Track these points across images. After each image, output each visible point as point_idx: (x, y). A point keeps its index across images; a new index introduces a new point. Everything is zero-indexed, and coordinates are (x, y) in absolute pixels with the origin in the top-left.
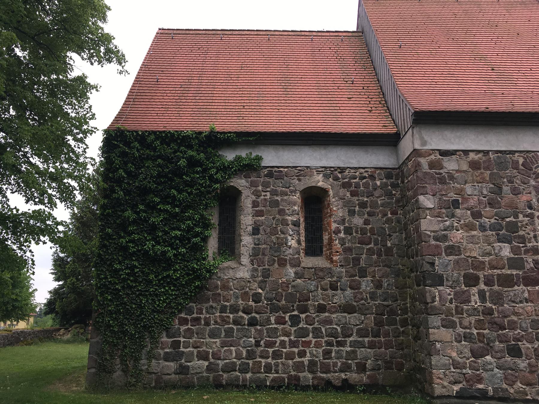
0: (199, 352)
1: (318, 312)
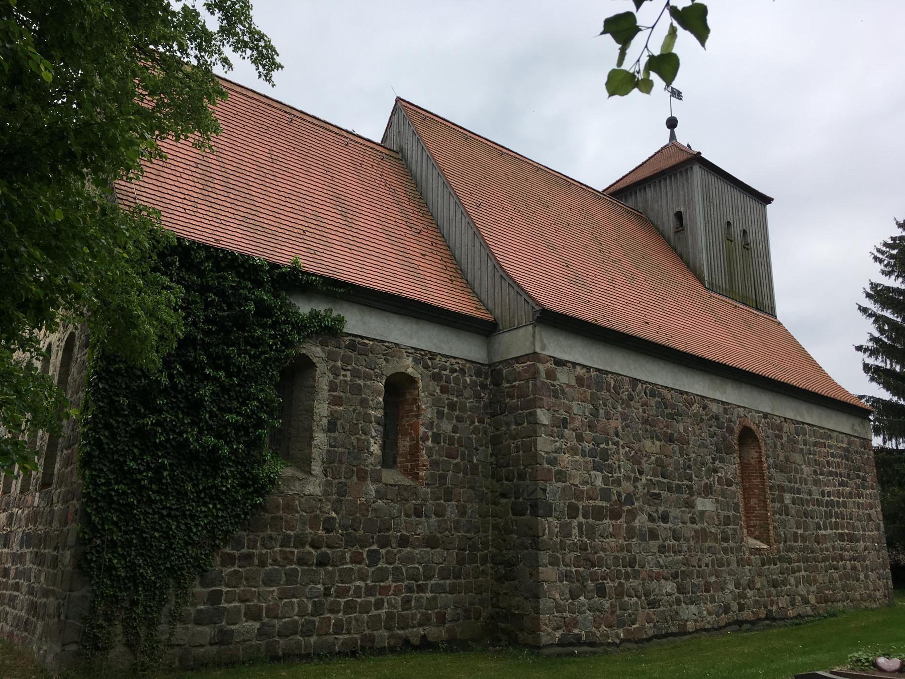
0: (248, 608)
1: (399, 546)
